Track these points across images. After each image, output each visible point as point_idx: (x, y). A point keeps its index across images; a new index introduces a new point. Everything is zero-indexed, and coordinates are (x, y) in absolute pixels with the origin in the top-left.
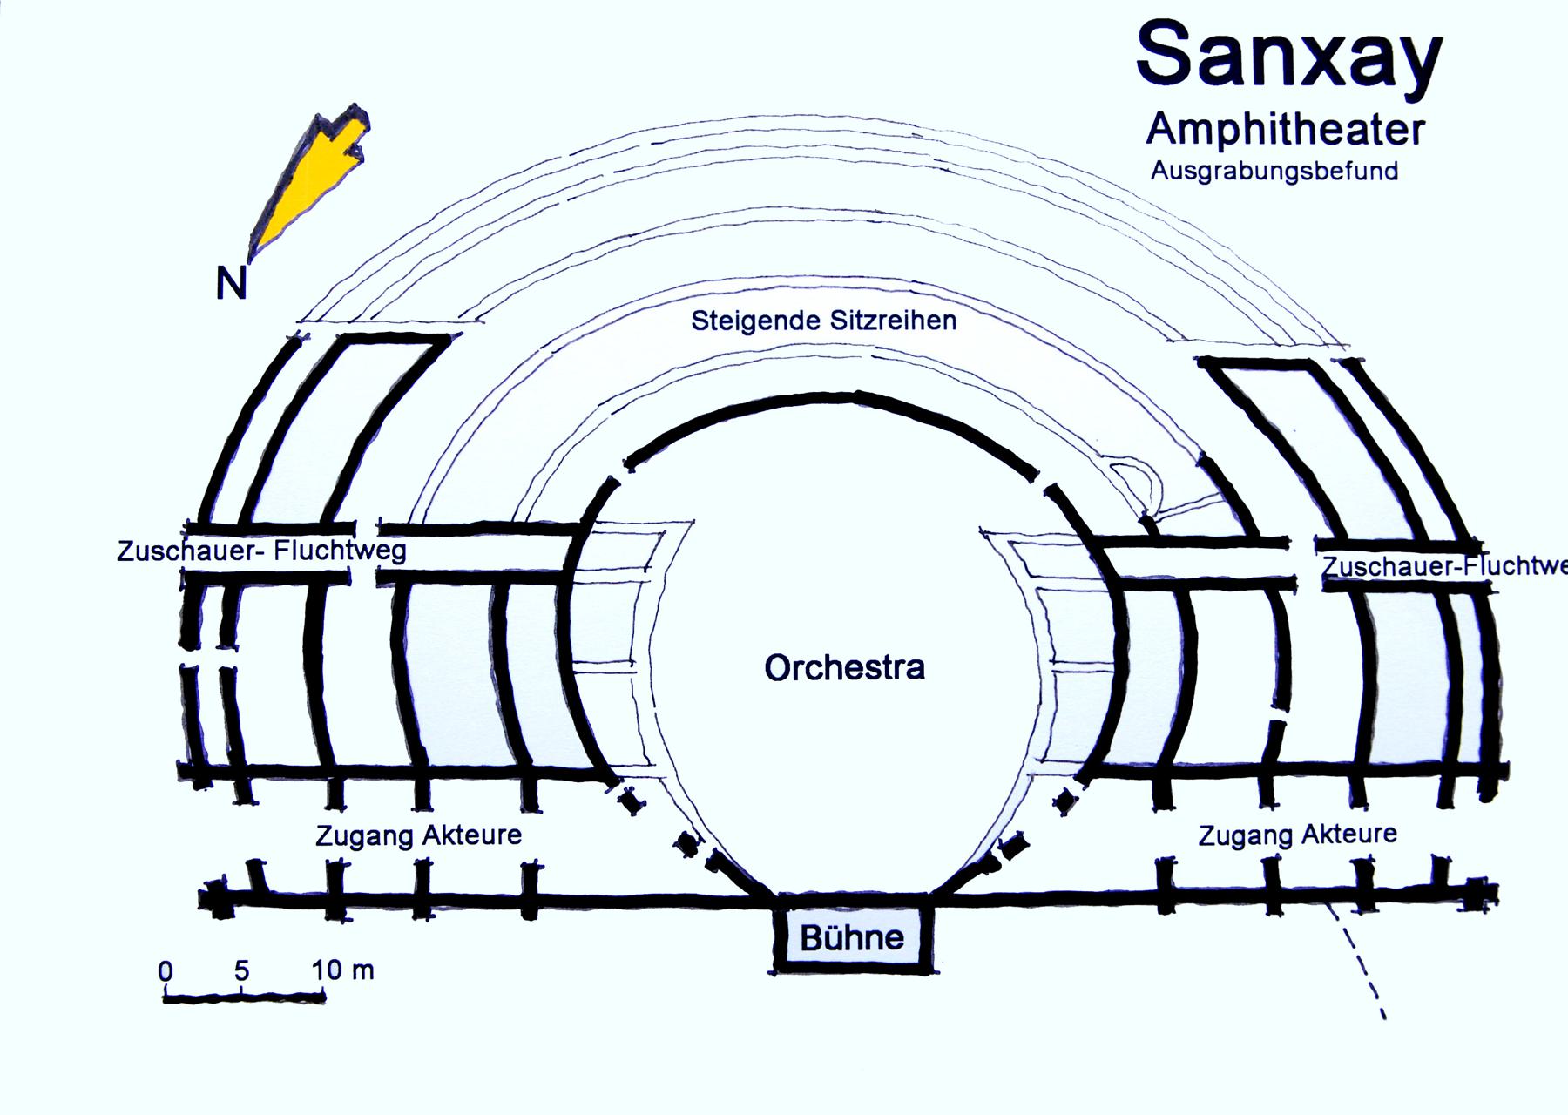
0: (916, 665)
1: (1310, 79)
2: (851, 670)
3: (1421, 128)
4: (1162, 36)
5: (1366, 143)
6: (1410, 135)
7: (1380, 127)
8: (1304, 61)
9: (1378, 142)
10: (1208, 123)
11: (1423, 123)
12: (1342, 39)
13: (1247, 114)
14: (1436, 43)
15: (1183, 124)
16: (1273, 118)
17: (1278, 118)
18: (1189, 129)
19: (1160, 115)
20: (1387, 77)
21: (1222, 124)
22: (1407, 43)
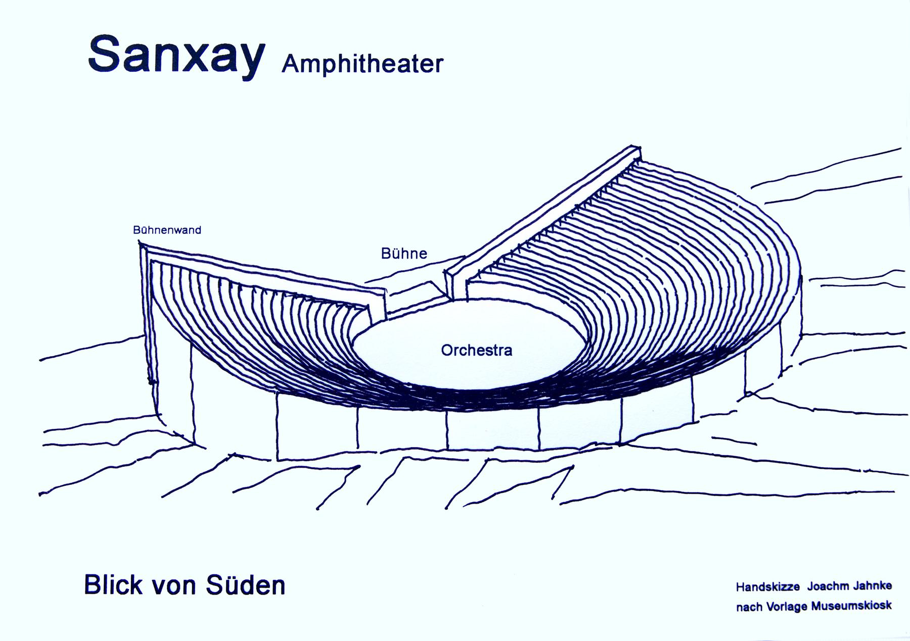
0: (508, 350)
1: (188, 68)
2: (480, 351)
3: (441, 63)
4: (104, 45)
5: (409, 71)
6: (434, 67)
7: (417, 62)
8: (185, 58)
9: (416, 71)
10: (317, 61)
11: (442, 60)
12: (207, 45)
13: (340, 55)
14: (262, 47)
15: (303, 61)
16: (355, 57)
17: (358, 58)
18: (307, 64)
19: (290, 56)
20: (232, 67)
21: (325, 61)
22: (245, 47)
